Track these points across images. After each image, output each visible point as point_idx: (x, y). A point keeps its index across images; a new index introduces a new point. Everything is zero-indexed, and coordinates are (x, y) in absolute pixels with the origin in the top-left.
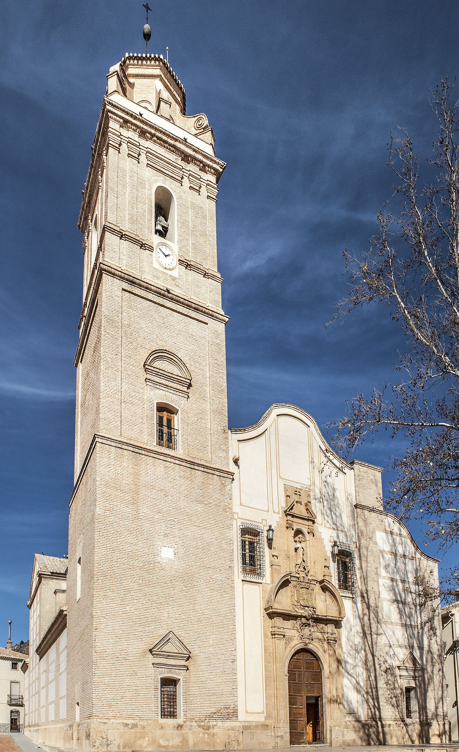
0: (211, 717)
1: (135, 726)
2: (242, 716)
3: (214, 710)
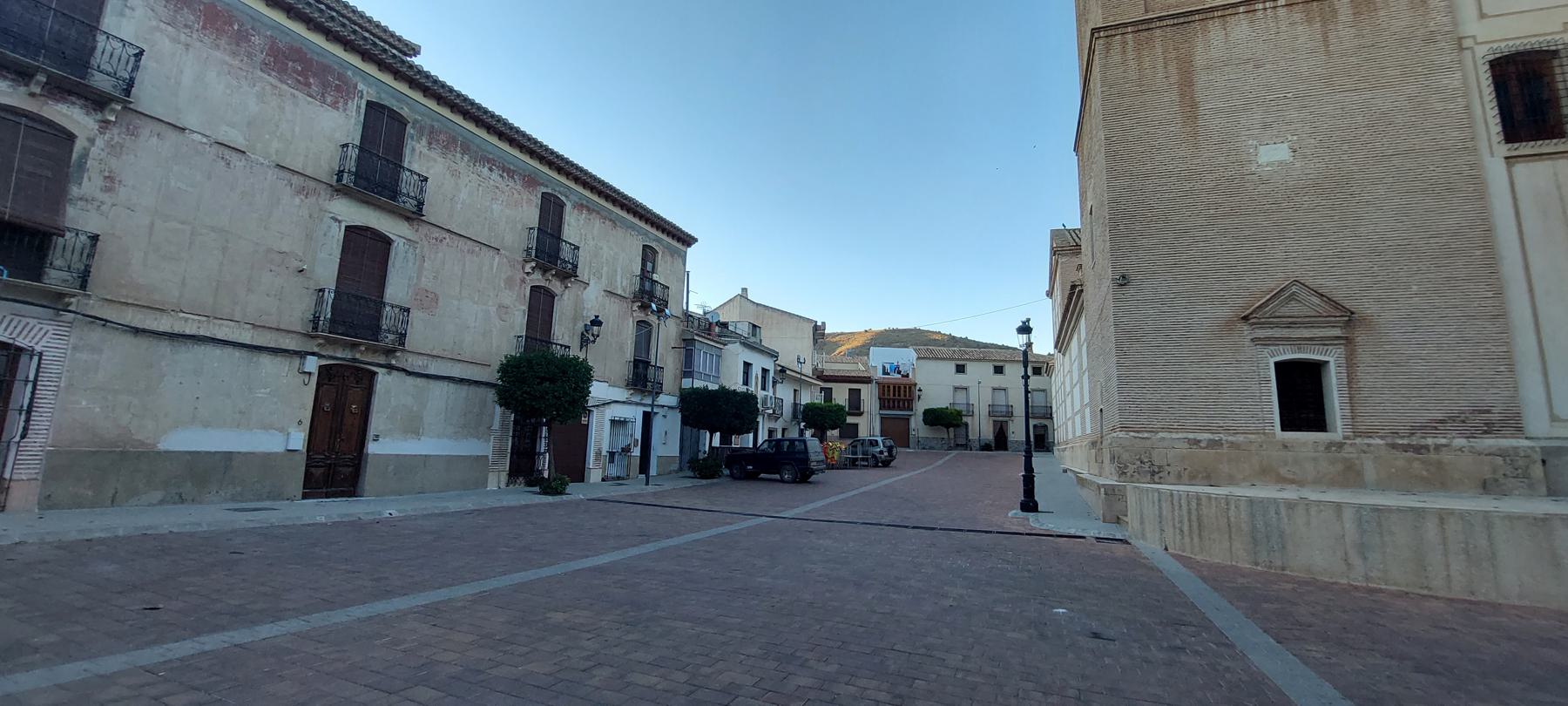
0: (1434, 426)
1: (1213, 444)
2: (1538, 424)
3: (1440, 416)
